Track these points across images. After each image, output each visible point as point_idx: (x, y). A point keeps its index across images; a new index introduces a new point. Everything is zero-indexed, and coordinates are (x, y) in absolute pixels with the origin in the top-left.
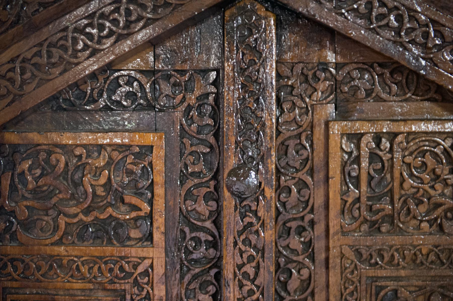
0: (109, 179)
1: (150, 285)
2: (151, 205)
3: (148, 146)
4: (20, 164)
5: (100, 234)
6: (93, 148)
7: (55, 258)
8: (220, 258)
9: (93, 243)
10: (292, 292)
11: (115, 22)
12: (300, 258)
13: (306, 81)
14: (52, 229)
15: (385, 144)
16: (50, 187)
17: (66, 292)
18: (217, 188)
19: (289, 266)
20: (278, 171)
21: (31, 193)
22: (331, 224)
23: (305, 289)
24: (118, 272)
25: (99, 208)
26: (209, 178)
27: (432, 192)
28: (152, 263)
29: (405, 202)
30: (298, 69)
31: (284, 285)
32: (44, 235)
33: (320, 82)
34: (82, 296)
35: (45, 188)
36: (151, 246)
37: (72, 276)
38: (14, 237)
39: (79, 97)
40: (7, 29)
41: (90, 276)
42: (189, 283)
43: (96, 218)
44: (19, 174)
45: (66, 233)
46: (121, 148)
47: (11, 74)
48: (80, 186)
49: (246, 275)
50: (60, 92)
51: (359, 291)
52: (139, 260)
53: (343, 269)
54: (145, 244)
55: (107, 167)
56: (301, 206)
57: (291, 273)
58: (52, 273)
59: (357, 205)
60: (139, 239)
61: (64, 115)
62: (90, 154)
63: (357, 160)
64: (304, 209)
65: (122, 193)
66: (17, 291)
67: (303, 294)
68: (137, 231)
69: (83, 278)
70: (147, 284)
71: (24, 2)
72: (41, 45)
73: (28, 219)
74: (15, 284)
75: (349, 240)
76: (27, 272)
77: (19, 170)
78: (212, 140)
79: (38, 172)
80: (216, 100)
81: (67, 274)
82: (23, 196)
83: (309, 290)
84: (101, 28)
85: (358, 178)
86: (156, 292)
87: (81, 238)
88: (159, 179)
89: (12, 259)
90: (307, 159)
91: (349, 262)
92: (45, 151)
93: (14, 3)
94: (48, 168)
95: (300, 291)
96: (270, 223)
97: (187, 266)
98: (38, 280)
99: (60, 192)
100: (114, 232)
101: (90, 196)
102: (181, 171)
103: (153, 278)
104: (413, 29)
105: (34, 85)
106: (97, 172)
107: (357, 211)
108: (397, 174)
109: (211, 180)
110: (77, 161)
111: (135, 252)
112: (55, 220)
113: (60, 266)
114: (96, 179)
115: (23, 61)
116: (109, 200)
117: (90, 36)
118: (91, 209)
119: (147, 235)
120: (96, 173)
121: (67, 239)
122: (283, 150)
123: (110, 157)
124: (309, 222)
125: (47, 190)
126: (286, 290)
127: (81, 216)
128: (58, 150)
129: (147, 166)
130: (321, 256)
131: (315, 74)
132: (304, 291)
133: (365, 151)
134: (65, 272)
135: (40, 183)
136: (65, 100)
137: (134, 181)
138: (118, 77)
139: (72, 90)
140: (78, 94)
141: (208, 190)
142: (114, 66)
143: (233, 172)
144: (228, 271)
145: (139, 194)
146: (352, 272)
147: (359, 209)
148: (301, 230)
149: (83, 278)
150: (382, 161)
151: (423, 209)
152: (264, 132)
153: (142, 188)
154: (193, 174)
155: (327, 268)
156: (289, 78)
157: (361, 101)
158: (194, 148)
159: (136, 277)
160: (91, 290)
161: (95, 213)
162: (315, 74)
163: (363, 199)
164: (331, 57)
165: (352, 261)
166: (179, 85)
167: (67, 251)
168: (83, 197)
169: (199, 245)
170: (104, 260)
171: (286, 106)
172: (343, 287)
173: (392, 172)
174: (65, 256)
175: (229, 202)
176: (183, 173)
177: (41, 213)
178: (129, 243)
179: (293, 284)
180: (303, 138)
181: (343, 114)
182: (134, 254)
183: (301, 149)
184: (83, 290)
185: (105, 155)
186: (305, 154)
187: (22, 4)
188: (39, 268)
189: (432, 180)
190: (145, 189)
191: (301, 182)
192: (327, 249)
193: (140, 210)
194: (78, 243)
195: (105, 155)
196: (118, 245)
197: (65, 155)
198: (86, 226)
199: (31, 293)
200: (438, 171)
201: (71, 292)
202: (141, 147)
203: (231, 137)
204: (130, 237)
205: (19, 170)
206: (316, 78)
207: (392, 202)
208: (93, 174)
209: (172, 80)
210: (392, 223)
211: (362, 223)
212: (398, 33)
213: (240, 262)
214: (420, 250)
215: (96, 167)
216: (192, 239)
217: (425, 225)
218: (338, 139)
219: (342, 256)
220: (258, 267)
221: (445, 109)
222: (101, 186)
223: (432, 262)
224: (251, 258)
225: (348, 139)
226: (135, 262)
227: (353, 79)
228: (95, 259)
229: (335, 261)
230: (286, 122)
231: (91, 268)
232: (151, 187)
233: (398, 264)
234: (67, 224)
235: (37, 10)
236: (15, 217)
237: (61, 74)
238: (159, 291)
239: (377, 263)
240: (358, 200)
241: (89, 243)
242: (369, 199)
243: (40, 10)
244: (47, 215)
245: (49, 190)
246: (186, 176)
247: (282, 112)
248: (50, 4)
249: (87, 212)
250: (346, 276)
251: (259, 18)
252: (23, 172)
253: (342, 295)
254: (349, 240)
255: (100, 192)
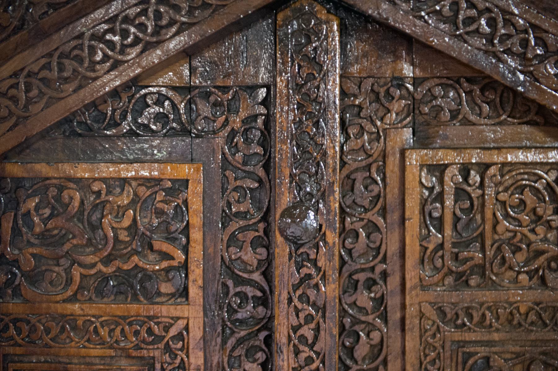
0: (134, 220)
1: (185, 351)
2: (186, 253)
3: (183, 180)
4: (24, 202)
5: (123, 288)
6: (115, 182)
7: (68, 318)
8: (271, 318)
9: (114, 300)
10: (359, 359)
12: (370, 318)
13: (377, 99)
14: (64, 282)
15: (475, 177)
16: (61, 230)
17: (82, 360)
18: (267, 232)
19: (357, 328)
20: (342, 210)
21: (38, 238)
22: (408, 277)
23: (376, 357)
24: (146, 335)
25: (122, 256)
26: (257, 219)
27: (532, 237)
28: (188, 324)
29: (499, 249)
30: (367, 85)
31: (350, 352)
32: (54, 289)
33: (394, 101)
34: (101, 364)
35: (56, 232)
36: (186, 303)
37: (88, 341)
38: (17, 292)
39: (97, 119)
40: (9, 36)
41: (111, 341)
42: (233, 349)
43: (119, 269)
44: (24, 215)
45: (81, 288)
46: (150, 182)
47: (13, 92)
48: (98, 229)
49: (303, 339)
50: (74, 114)
51: (442, 358)
52: (171, 321)
53: (423, 332)
54: (179, 300)
55: (132, 206)
56: (371, 254)
57: (359, 336)
58: (64, 336)
59: (440, 253)
60: (171, 294)
61: (79, 142)
62: (111, 189)
63: (440, 198)
64: (375, 257)
65: (151, 238)
66: (21, 358)
67: (373, 362)
68: (169, 285)
69: (103, 343)
70: (181, 350)
71: (30, 3)
72: (50, 55)
73: (35, 270)
74: (18, 351)
75: (430, 296)
76: (33, 336)
77: (23, 210)
78: (261, 172)
79: (47, 212)
80: (267, 123)
81: (83, 337)
82: (28, 241)
83: (381, 358)
84: (125, 34)
85: (441, 219)
86: (192, 360)
87: (100, 293)
88: (196, 220)
89: (15, 319)
90: (378, 196)
91: (430, 322)
92: (55, 186)
93: (17, 4)
94: (59, 207)
95: (370, 359)
96: (333, 275)
97: (230, 328)
98: (47, 346)
99: (74, 237)
100: (141, 286)
101: (111, 242)
102: (224, 211)
103: (188, 343)
104: (509, 36)
105: (42, 105)
106: (120, 212)
107: (440, 260)
108: (489, 214)
109: (260, 221)
110: (95, 199)
111: (166, 310)
112: (68, 271)
113: (75, 328)
114: (119, 220)
115: (29, 75)
116: (134, 247)
117: (111, 45)
118: (112, 257)
119: (181, 289)
120: (118, 213)
121: (83, 295)
122: (349, 185)
123: (135, 194)
124: (381, 273)
125: (58, 234)
126: (352, 358)
127: (100, 266)
128: (72, 185)
129: (181, 204)
130: (395, 316)
131: (387, 92)
132: (374, 358)
133: (449, 187)
134: (81, 336)
135: (49, 226)
136: (80, 123)
137: (165, 224)
138: (145, 95)
139: (88, 111)
140: (96, 115)
141: (257, 234)
142: (141, 81)
143: (287, 212)
144: (281, 334)
145: (171, 239)
146: (434, 336)
147: (442, 257)
148: (370, 284)
149: (103, 343)
150: (471, 199)
151: (521, 257)
152: (325, 163)
153: (174, 232)
154: (237, 214)
155: (403, 330)
156: (356, 96)
157: (445, 124)
158: (238, 183)
159: (168, 341)
160: (112, 357)
161: (117, 263)
162: (387, 92)
163: (448, 245)
164: (408, 70)
165: (434, 322)
166: (221, 104)
167: (82, 310)
168: (103, 242)
169: (245, 302)
170: (128, 321)
171: (352, 131)
172: (422, 354)
173: (483, 213)
174: (80, 316)
175: (282, 249)
176: (226, 213)
177: (51, 262)
178: (158, 300)
179: (362, 350)
180: (373, 170)
181: (423, 141)
182: (165, 313)
183: (371, 184)
184: (102, 357)
185: (129, 192)
186: (376, 189)
187: (27, 6)
188: (48, 331)
189: (532, 222)
190: (179, 234)
191: (370, 224)
192: (403, 307)
193: (173, 258)
194: (96, 299)
195: (129, 191)
196: (145, 302)
197: (81, 191)
198: (106, 279)
199: (39, 362)
200: (540, 211)
201: (88, 360)
202: (173, 181)
203: (284, 169)
204: (160, 292)
205: (23, 210)
206: (390, 96)
207: (483, 249)
208: (114, 215)
209: (212, 99)
210: (483, 275)
211: (446, 275)
212: (490, 41)
213: (295, 323)
214: (518, 309)
215: (119, 206)
216: (237, 294)
217: (523, 277)
218: (416, 171)
219: (422, 315)
220: (317, 330)
221: (548, 134)
222: (125, 229)
223: (532, 323)
224: (309, 319)
225: (429, 171)
226: (167, 322)
227: (435, 98)
228: (117, 319)
229: (412, 322)
230: (352, 151)
231: (112, 331)
232: (186, 230)
233: (491, 326)
234: (83, 276)
235: (46, 13)
236: (19, 268)
237: (75, 91)
238: (196, 359)
239: (464, 325)
240: (441, 246)
241: (110, 300)
242: (454, 245)
243: (49, 13)
244: (58, 265)
245: (61, 234)
246: (229, 216)
247: (347, 138)
248: (61, 5)
249: (107, 261)
250: (426, 340)
251: (319, 23)
252: (29, 212)
253: (421, 363)
254: (430, 296)
255: (124, 236)
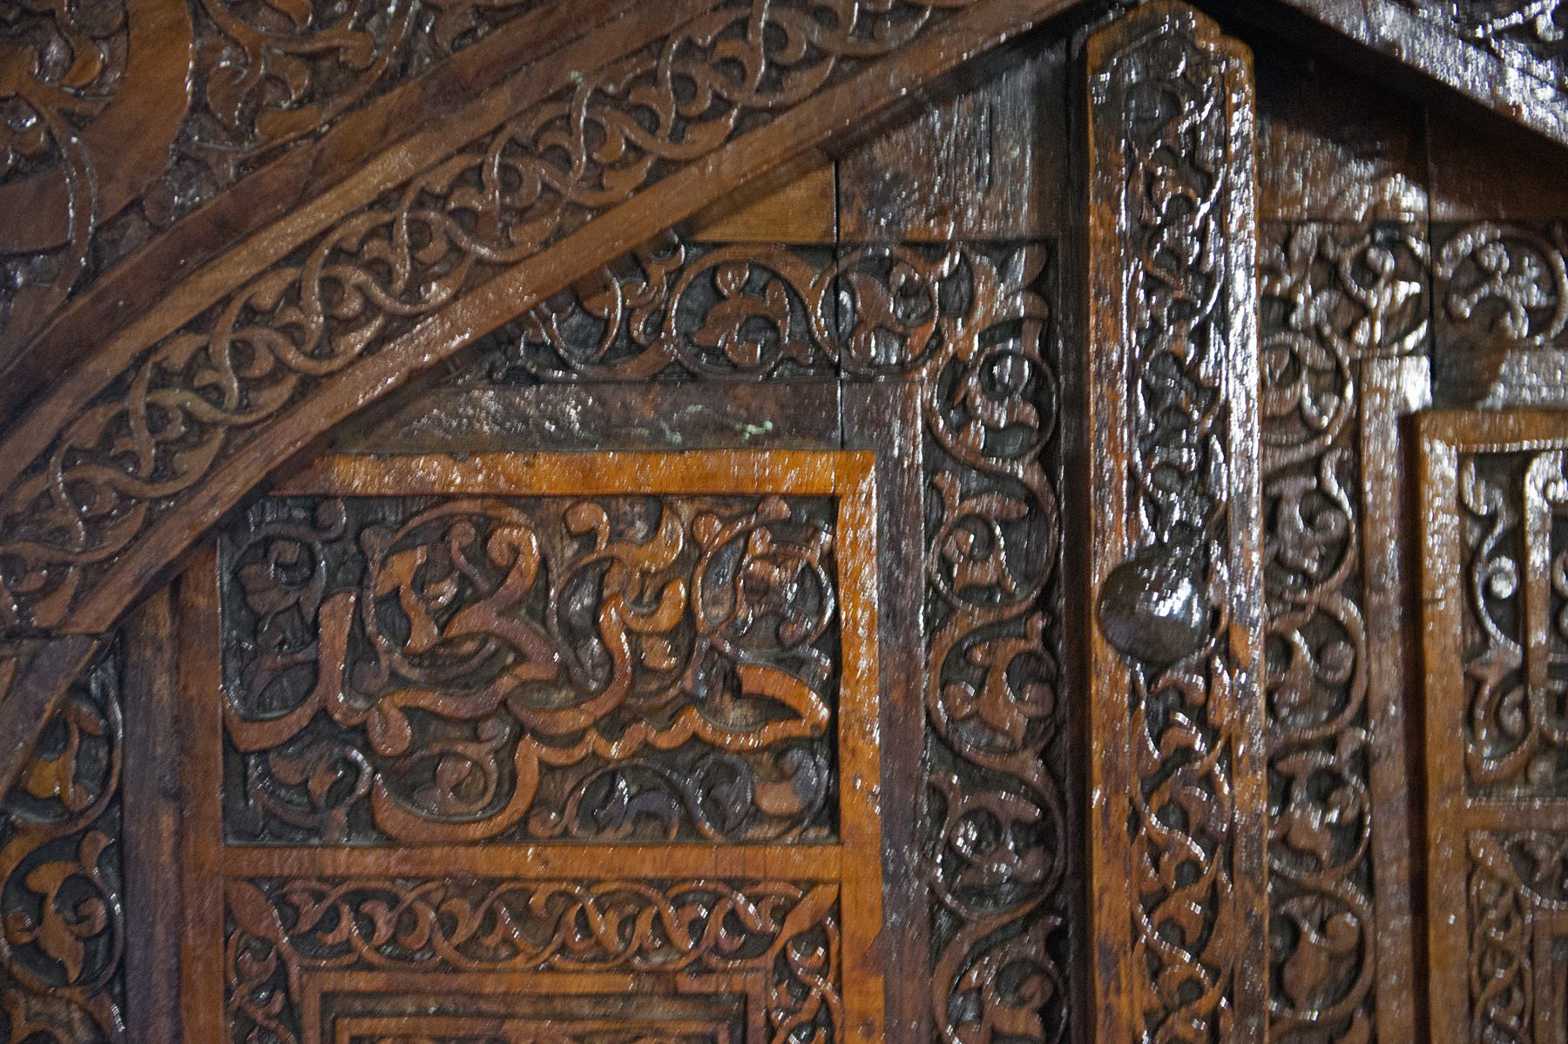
0: (689, 611)
1: (831, 976)
2: (833, 702)
3: (817, 497)
4: (384, 563)
5: (655, 801)
6: (632, 506)
7: (504, 887)
9: (633, 834)
11: (382, 270)
14: (492, 788)
16: (485, 642)
17: (543, 1007)
19: (1293, 907)
21: (420, 665)
23: (1344, 987)
24: (723, 932)
25: (652, 713)
26: (1024, 606)
28: (838, 900)
32: (462, 808)
33: (1382, 283)
34: (594, 1018)
35: (469, 647)
36: (833, 839)
37: (563, 949)
38: (364, 819)
39: (581, 336)
40: (369, 96)
41: (625, 950)
43: (647, 745)
44: (380, 601)
45: (539, 803)
46: (729, 506)
47: (374, 248)
48: (587, 638)
49: (1172, 928)
50: (521, 321)
51: (1528, 988)
52: (792, 890)
53: (1475, 912)
54: (812, 834)
55: (681, 572)
56: (1326, 703)
58: (490, 941)
59: (1515, 696)
60: (790, 816)
62: (621, 527)
63: (1515, 544)
64: (1335, 713)
65: (734, 661)
66: (371, 1005)
67: (1335, 1003)
68: (785, 788)
69: (603, 955)
70: (823, 971)
71: (427, 6)
72: (477, 146)
73: (412, 753)
74: (362, 981)
75: (1498, 808)
76: (409, 941)
77: (381, 584)
79: (447, 591)
81: (548, 942)
82: (394, 674)
87: (595, 816)
89: (355, 892)
90: (1344, 542)
91: (1495, 887)
92: (469, 517)
93: (392, 9)
94: (485, 574)
95: (1326, 992)
97: (951, 913)
99: (522, 658)
100: (706, 796)
102: (931, 583)
103: (839, 952)
106: (653, 589)
107: (1517, 714)
109: (1032, 611)
110: (577, 553)
113: (523, 916)
114: (645, 610)
116: (688, 684)
118: (625, 715)
119: (819, 802)
120: (642, 594)
121: (545, 821)
123: (691, 539)
124: (1354, 754)
125: (476, 652)
128: (515, 515)
129: (815, 564)
132: (1339, 993)
134: (539, 938)
135: (454, 631)
136: (535, 347)
137: (772, 621)
139: (559, 312)
140: (579, 326)
141: (1022, 645)
142: (704, 228)
145: (792, 664)
146: (1505, 923)
147: (1524, 706)
153: (795, 645)
159: (784, 950)
160: (627, 997)
161: (641, 731)
162: (1361, 262)
163: (1538, 670)
164: (1412, 200)
165: (1504, 887)
167: (546, 863)
168: (600, 673)
169: (991, 837)
170: (674, 892)
172: (1474, 973)
174: (537, 880)
175: (1112, 678)
176: (936, 590)
177: (455, 733)
178: (754, 833)
182: (774, 871)
183: (1321, 509)
184: (599, 998)
185: (674, 530)
186: (1334, 524)
187: (418, 14)
188: (448, 924)
190: (812, 646)
191: (1321, 621)
193: (795, 715)
194: (581, 834)
195: (674, 532)
196: (719, 838)
197: (540, 531)
199: (421, 1013)
201: (558, 1005)
202: (792, 499)
203: (1116, 457)
204: (758, 810)
205: (381, 584)
206: (1368, 273)
208: (633, 597)
211: (1533, 756)
215: (645, 574)
219: (1473, 867)
220: (1213, 901)
222: (663, 635)
225: (1480, 473)
226: (779, 896)
228: (643, 889)
229: (1445, 882)
234: (547, 768)
235: (473, 30)
236: (367, 748)
238: (865, 997)
240: (1520, 676)
241: (621, 834)
243: (480, 33)
244: (476, 738)
245: (485, 652)
246: (945, 599)
248: (513, 13)
249: (613, 725)
250: (1485, 935)
251: (1203, 61)
252: (396, 591)
253: (1472, 1002)
254: (1498, 808)
